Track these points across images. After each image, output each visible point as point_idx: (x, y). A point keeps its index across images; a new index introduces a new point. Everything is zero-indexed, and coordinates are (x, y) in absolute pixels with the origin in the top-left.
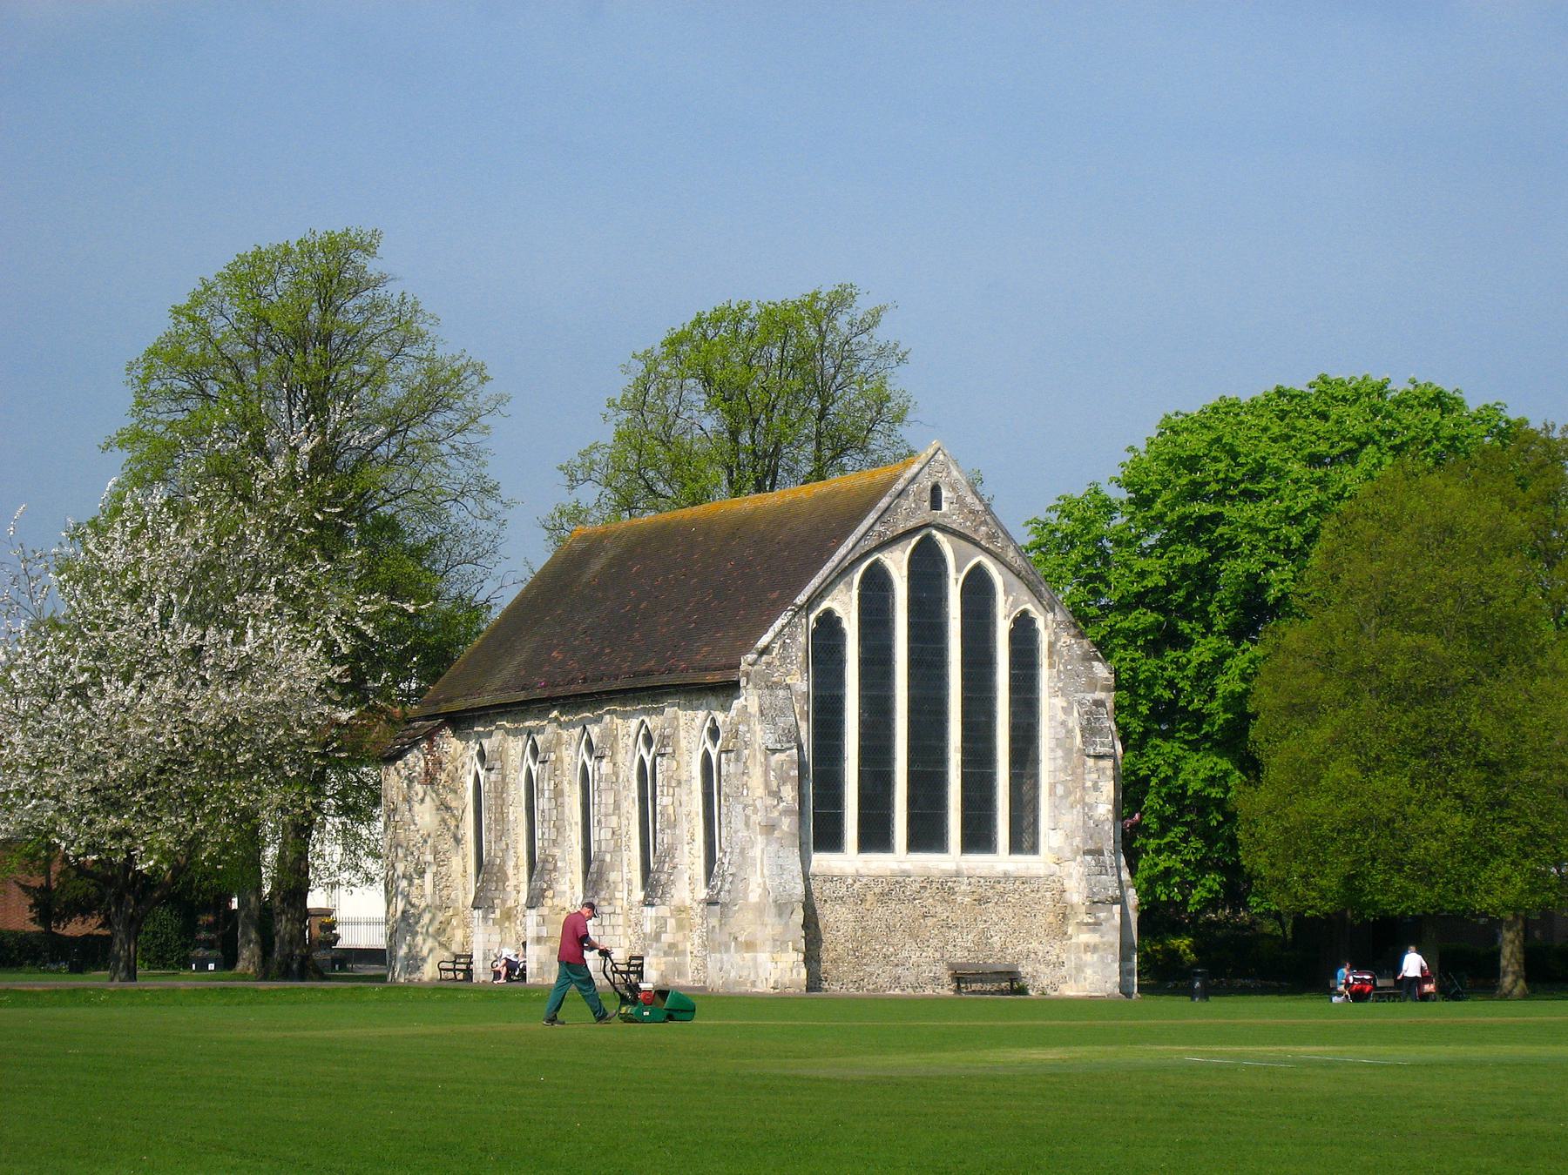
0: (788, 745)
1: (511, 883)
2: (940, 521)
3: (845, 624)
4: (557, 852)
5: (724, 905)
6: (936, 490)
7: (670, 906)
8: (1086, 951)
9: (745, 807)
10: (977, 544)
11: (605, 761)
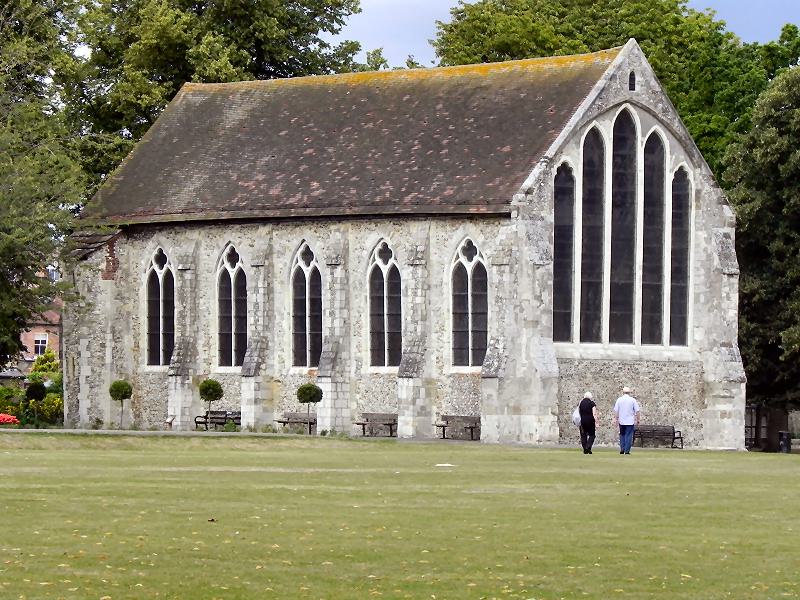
0: (547, 262)
1: (202, 356)
2: (635, 98)
3: (574, 174)
4: (268, 334)
5: (501, 379)
6: (632, 76)
7: (422, 378)
8: (730, 413)
9: (515, 307)
10: (655, 116)
11: (339, 268)
